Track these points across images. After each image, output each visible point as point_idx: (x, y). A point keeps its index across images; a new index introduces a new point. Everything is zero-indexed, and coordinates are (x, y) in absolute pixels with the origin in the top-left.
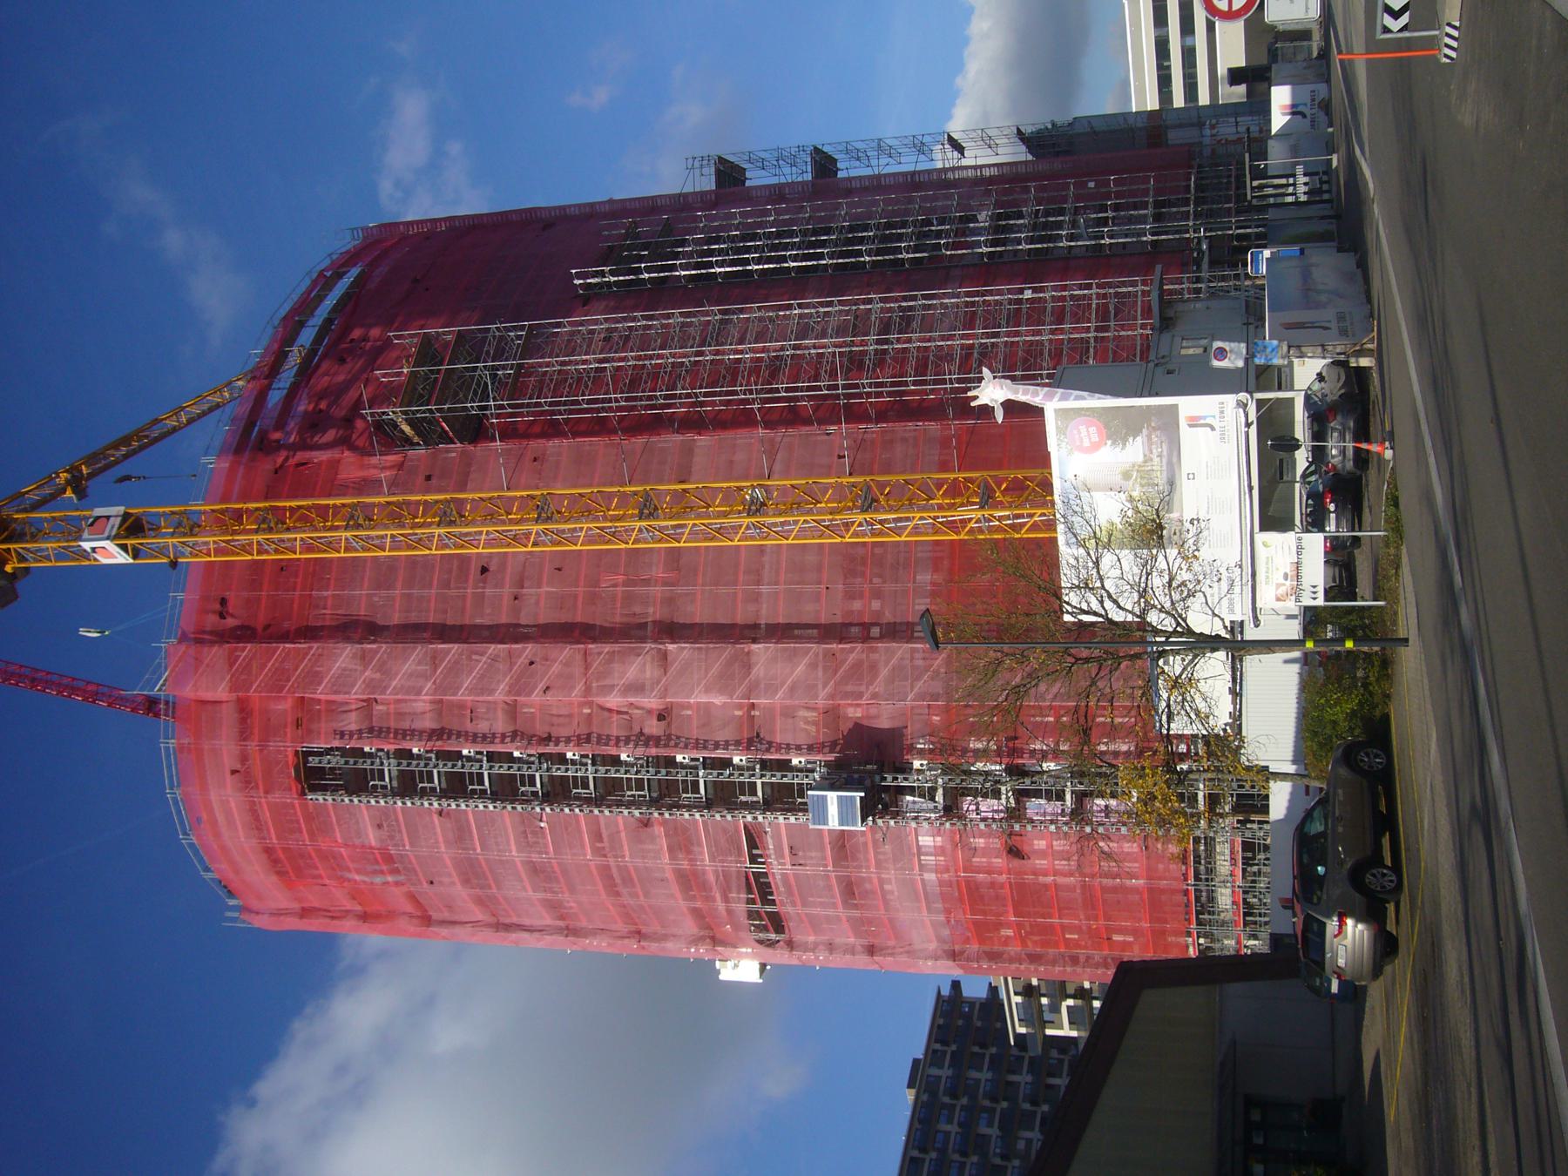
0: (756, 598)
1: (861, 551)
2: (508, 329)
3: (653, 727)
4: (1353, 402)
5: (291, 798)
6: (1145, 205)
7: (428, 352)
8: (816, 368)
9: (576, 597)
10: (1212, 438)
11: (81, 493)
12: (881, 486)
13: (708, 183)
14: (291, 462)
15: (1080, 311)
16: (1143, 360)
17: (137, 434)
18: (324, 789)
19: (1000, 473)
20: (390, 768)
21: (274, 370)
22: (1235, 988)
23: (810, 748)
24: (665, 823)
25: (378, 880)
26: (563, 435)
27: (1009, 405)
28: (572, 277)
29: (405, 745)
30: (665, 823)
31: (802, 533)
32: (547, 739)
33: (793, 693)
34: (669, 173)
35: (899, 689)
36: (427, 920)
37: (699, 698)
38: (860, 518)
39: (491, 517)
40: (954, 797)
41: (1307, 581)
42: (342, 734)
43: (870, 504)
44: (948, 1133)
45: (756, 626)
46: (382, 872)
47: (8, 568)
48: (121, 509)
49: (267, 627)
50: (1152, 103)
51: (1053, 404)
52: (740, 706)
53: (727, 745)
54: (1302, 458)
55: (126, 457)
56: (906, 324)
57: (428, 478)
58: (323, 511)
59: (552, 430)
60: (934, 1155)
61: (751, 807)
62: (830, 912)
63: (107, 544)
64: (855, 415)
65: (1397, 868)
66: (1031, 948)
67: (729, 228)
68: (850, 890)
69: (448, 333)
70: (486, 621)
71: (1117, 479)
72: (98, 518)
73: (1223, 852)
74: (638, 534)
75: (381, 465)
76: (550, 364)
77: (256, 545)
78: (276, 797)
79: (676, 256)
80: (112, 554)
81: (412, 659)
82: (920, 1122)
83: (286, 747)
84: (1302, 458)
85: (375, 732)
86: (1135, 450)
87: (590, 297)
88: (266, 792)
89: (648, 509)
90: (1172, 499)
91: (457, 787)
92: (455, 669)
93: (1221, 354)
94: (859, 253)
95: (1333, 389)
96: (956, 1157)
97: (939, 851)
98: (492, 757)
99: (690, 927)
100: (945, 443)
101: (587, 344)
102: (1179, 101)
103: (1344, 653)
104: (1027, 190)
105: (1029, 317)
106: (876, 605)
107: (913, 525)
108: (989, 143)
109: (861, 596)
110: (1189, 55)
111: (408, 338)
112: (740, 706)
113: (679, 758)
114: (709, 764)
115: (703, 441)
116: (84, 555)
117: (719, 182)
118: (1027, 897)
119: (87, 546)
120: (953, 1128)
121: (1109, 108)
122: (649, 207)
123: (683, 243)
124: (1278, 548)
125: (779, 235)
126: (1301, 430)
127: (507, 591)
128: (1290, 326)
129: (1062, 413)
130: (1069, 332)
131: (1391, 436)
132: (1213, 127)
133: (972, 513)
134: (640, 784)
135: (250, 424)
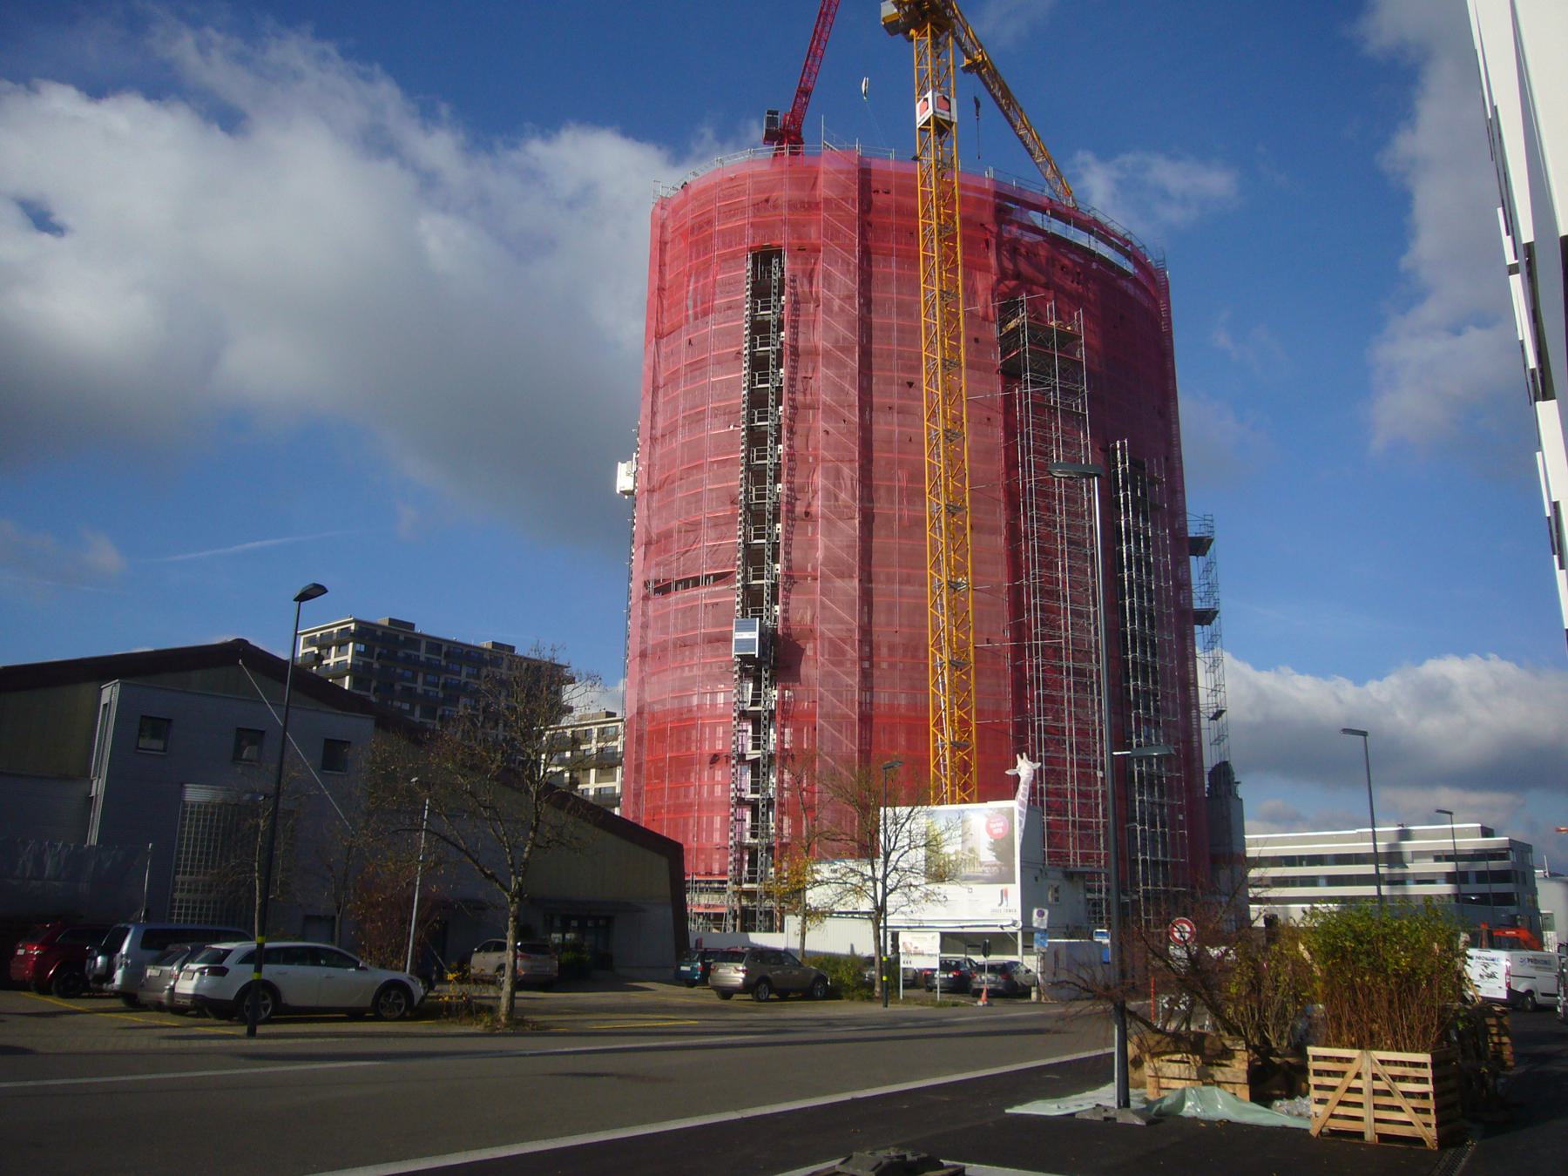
0: (890, 579)
1: (922, 655)
3: (800, 509)
4: (1011, 987)
5: (748, 242)
6: (1164, 855)
7: (1068, 340)
8: (1050, 622)
10: (994, 905)
11: (967, 69)
12: (967, 674)
13: (1193, 531)
15: (1087, 810)
16: (1047, 862)
18: (755, 264)
19: (975, 756)
20: (770, 315)
21: (1057, 215)
22: (669, 912)
23: (786, 619)
24: (734, 516)
25: (690, 303)
26: (1006, 440)
27: (1017, 778)
28: (1122, 440)
29: (786, 327)
30: (734, 516)
31: (934, 542)
32: (791, 431)
33: (823, 612)
35: (826, 679)
36: (659, 336)
37: (821, 540)
38: (944, 580)
39: (948, 393)
40: (755, 719)
41: (913, 958)
42: (793, 281)
43: (955, 665)
44: (459, 673)
45: (871, 581)
46: (695, 306)
47: (912, 32)
48: (955, 120)
49: (870, 225)
51: (1016, 806)
52: (814, 569)
53: (789, 561)
54: (979, 959)
55: (994, 96)
56: (1081, 687)
57: (976, 340)
58: (954, 270)
59: (1010, 431)
60: (443, 663)
61: (745, 578)
62: (671, 629)
63: (930, 112)
64: (1018, 652)
65: (768, 1000)
66: (644, 767)
67: (1156, 552)
68: (684, 644)
69: (1081, 354)
70: (874, 388)
71: (970, 844)
73: (714, 899)
74: (934, 504)
75: (985, 303)
76: (1056, 431)
77: (928, 224)
78: (749, 232)
79: (1136, 516)
80: (923, 112)
81: (844, 331)
82: (468, 653)
83: (783, 238)
84: (979, 959)
85: (796, 304)
86: (987, 856)
88: (752, 225)
89: (952, 510)
90: (956, 877)
91: (759, 365)
92: (841, 365)
93: (1041, 914)
94: (1134, 651)
95: (1020, 978)
96: (442, 681)
97: (714, 705)
98: (779, 389)
99: (657, 527)
100: (997, 713)
101: (1071, 453)
103: (877, 976)
104: (1178, 770)
105: (1084, 774)
106: (884, 665)
107: (941, 696)
108: (1219, 740)
109: (890, 656)
111: (1078, 323)
112: (814, 569)
113: (779, 526)
114: (776, 546)
115: (1001, 541)
116: (923, 91)
117: (1192, 539)
118: (684, 765)
119: (929, 95)
120: (463, 678)
121: (1246, 824)
122: (1175, 488)
123: (1145, 520)
125: (1149, 590)
126: (994, 958)
127: (896, 402)
128: (1056, 955)
129: (1011, 810)
130: (1073, 802)
131: (989, 1005)
133: (947, 737)
134: (761, 497)
135: (1017, 201)
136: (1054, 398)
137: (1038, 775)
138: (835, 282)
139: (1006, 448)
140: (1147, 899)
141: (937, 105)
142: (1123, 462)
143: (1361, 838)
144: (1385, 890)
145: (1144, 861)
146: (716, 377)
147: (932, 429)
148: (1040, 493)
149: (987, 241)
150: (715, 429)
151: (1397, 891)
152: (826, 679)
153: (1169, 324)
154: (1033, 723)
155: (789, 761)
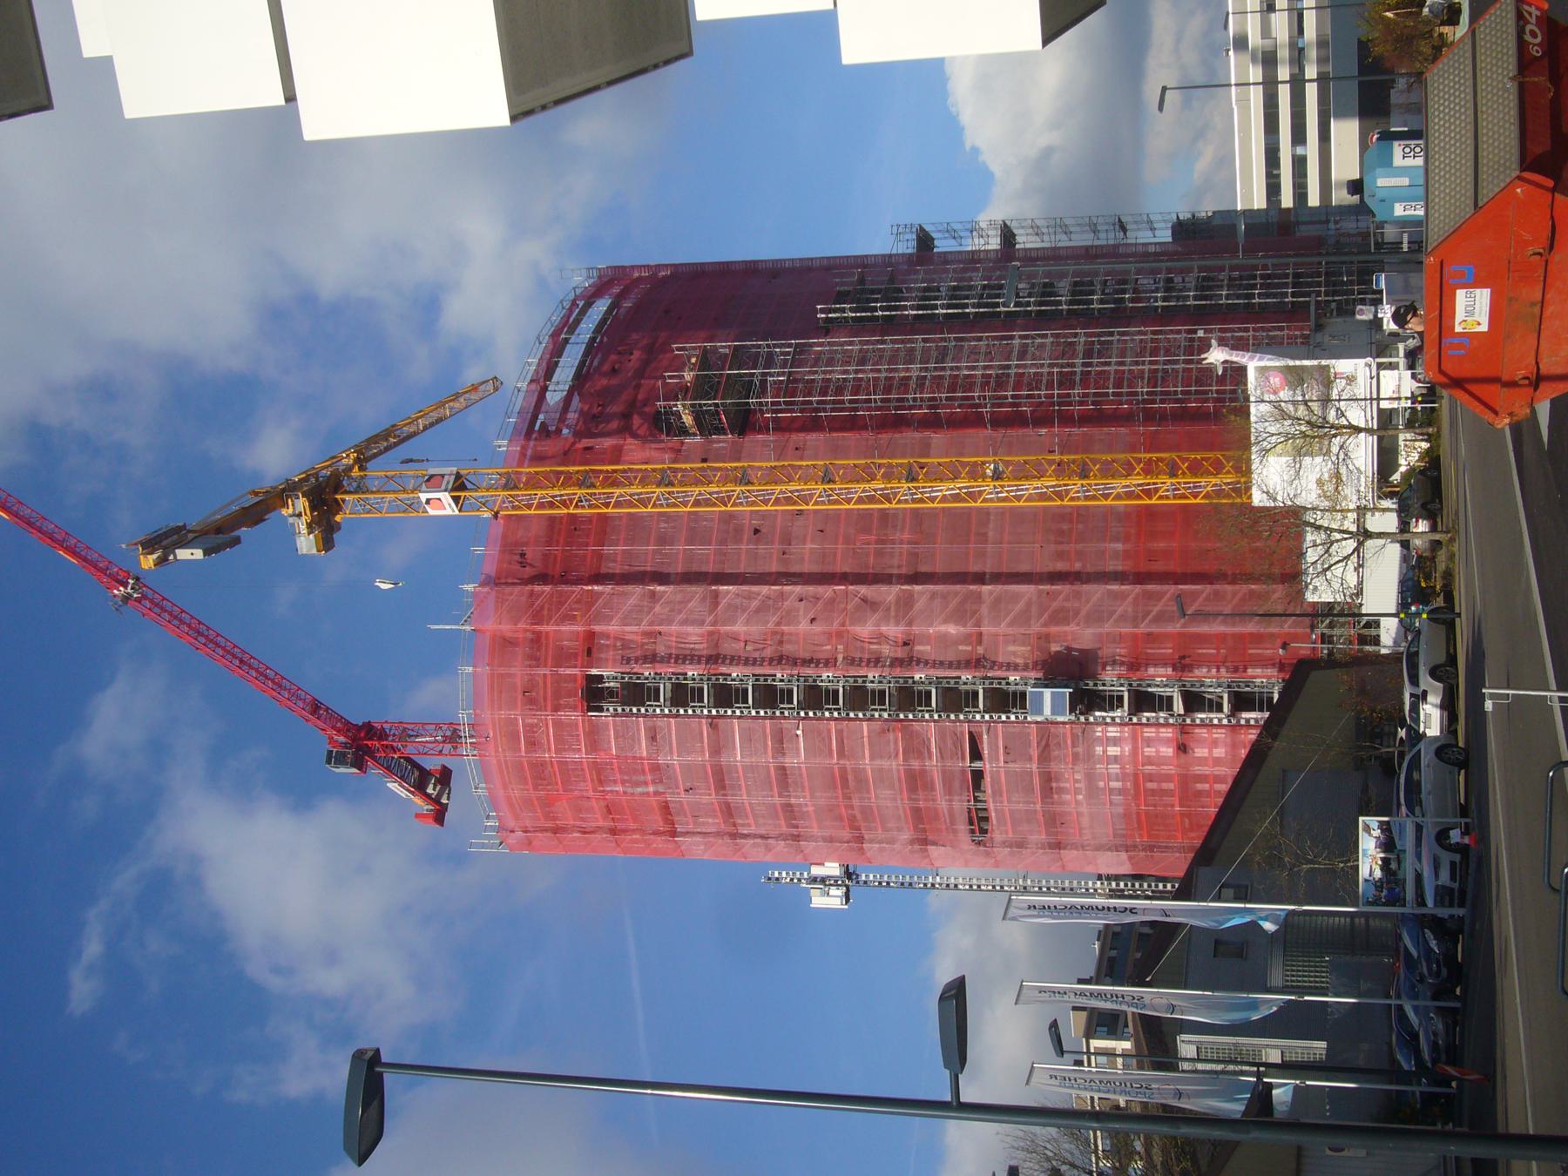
2: (775, 346)
9: (835, 554)
11: (361, 468)
14: (580, 446)
17: (386, 434)
23: (1026, 668)
33: (1010, 630)
34: (877, 236)
35: (1098, 622)
45: (984, 574)
48: (455, 469)
50: (1259, 202)
51: (1253, 364)
59: (813, 425)
64: (1067, 420)
72: (432, 476)
74: (904, 495)
87: (828, 328)
102: (1287, 200)
110: (1300, 164)
111: (689, 350)
122: (863, 264)
124: (1398, 160)
127: (777, 546)
129: (1262, 370)
132: (1336, 222)
136: (777, 376)
137: (1222, 343)
138: (624, 617)
139: (831, 430)
140: (1334, 293)
141: (437, 488)
142: (843, 310)
143: (1244, 102)
144: (1311, 72)
145: (1293, 295)
146: (737, 756)
147: (819, 497)
148: (888, 390)
149: (587, 449)
150: (798, 758)
151: (1312, 53)
152: (1098, 622)
153: (659, 267)
154: (1144, 401)
155: (1187, 661)
